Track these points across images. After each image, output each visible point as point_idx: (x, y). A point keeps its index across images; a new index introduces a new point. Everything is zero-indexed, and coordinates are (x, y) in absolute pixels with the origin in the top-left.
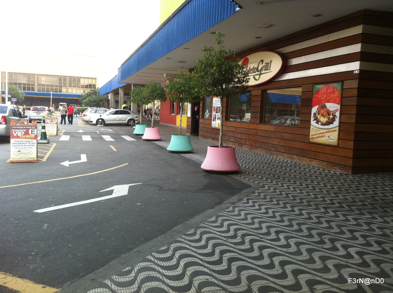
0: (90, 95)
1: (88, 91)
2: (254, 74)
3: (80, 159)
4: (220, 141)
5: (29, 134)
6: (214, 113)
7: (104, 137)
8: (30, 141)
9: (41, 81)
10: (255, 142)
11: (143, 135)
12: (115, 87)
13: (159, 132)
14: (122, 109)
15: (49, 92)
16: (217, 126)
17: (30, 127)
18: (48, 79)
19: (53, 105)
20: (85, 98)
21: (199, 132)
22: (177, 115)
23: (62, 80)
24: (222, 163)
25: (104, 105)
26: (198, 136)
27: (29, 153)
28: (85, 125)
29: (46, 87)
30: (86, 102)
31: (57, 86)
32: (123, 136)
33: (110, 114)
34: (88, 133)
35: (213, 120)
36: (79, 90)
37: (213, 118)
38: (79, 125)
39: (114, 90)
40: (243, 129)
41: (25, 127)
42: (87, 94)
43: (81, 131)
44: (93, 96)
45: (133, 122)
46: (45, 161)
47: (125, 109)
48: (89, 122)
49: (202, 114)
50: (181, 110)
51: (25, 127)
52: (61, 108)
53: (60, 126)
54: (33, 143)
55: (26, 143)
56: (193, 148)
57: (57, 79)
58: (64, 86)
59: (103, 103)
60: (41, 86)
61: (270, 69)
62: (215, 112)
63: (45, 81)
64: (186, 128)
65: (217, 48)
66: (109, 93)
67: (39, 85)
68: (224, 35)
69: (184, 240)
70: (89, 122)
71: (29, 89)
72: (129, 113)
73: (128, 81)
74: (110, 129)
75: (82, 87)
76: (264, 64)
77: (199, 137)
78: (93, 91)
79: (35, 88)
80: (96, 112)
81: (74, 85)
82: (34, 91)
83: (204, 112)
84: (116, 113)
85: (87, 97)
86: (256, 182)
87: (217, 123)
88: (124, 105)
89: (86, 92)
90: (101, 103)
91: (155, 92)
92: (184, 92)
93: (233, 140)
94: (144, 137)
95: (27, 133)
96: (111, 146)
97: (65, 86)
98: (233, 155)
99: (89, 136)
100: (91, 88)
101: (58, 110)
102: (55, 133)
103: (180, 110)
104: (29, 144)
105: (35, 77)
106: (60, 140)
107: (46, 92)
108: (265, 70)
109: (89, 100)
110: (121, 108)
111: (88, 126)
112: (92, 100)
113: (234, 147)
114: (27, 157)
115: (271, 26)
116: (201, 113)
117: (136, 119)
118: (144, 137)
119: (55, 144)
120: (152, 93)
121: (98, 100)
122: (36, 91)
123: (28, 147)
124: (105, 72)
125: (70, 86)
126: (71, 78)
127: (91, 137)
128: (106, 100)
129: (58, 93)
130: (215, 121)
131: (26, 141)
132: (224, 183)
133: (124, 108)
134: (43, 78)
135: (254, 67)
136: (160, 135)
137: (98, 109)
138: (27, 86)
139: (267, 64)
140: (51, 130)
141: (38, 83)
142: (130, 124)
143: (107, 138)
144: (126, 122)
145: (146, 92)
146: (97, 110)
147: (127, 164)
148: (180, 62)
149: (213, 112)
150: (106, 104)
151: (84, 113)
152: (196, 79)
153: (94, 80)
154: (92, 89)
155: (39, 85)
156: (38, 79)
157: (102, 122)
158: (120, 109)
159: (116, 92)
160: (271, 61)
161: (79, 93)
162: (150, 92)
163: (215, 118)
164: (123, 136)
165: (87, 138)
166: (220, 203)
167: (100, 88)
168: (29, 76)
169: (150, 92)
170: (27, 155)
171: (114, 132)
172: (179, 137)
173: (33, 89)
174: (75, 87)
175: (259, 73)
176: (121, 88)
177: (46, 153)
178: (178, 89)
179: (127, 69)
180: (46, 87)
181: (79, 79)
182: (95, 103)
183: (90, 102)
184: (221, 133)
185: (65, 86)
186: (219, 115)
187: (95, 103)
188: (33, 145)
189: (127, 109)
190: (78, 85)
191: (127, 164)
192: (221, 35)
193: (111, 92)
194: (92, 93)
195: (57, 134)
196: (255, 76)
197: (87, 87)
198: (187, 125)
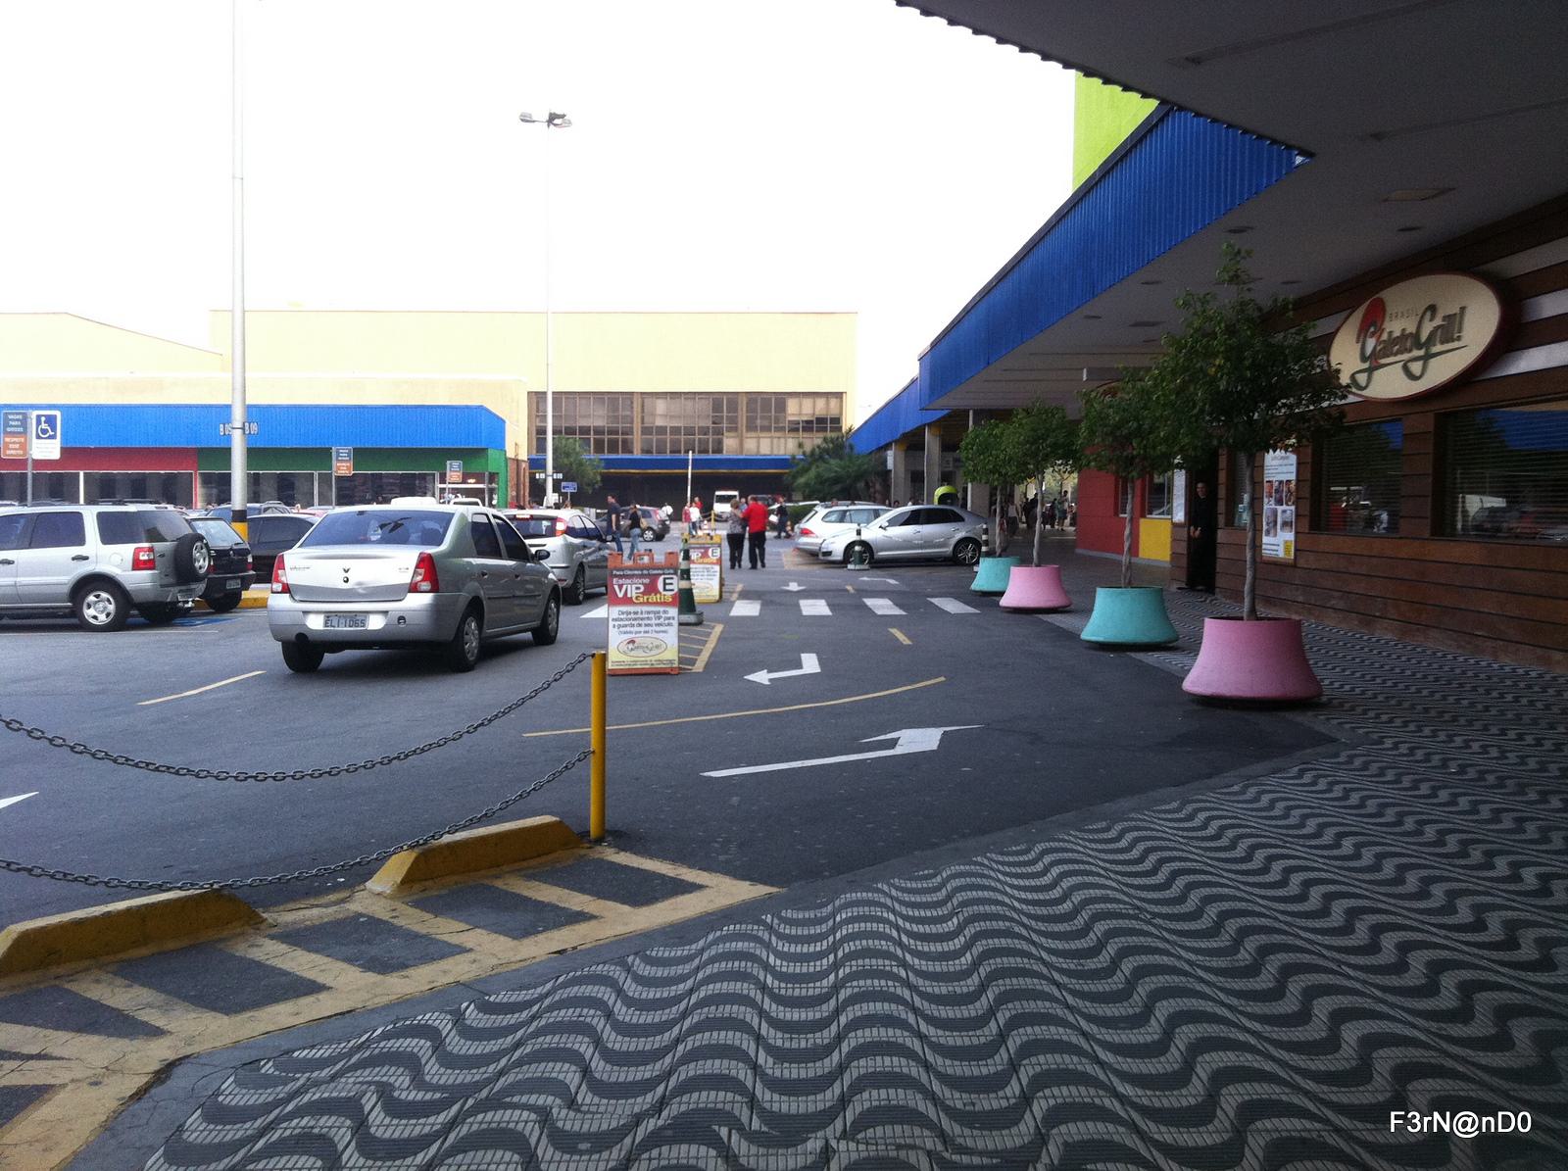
0: (821, 457)
1: (813, 441)
2: (1406, 356)
3: (799, 666)
4: (1247, 601)
5: (657, 591)
6: (1268, 505)
7: (869, 602)
8: (659, 612)
9: (653, 415)
10: (1418, 606)
11: (1001, 594)
12: (909, 424)
13: (1059, 580)
14: (935, 505)
15: (679, 452)
16: (1281, 554)
17: (660, 572)
18: (676, 406)
19: (697, 499)
20: (806, 470)
21: (1218, 577)
22: (1143, 516)
23: (724, 406)
24: (1251, 671)
25: (872, 490)
26: (1214, 594)
27: (657, 647)
28: (805, 568)
29: (668, 437)
30: (807, 484)
31: (704, 431)
32: (935, 601)
33: (892, 522)
34: (820, 591)
35: (1268, 533)
36: (782, 440)
37: (1268, 524)
38: (786, 568)
39: (905, 436)
40: (1374, 560)
41: (645, 572)
42: (813, 452)
43: (794, 587)
44: (832, 462)
45: (974, 550)
46: (701, 670)
47: (946, 504)
48: (821, 557)
49: (1227, 509)
50: (1129, 501)
51: (645, 572)
52: (720, 508)
53: (729, 576)
54: (669, 618)
55: (648, 618)
56: (1175, 631)
57: (706, 406)
58: (730, 430)
59: (867, 484)
60: (651, 434)
61: (1459, 338)
62: (1272, 502)
63: (666, 416)
64: (1168, 565)
65: (1227, 298)
66: (887, 446)
67: (646, 431)
68: (1249, 253)
69: (1074, 841)
70: (821, 557)
71: (613, 448)
72: (961, 519)
73: (954, 400)
74: (892, 577)
75: (794, 428)
76: (1438, 321)
77: (1218, 596)
78: (832, 441)
79: (632, 443)
80: (842, 520)
81: (766, 423)
82: (631, 452)
83: (1233, 500)
84: (913, 519)
85: (811, 464)
86: (1361, 731)
87: (1278, 543)
88: (940, 491)
89: (808, 448)
90: (861, 485)
91: (1045, 440)
92: (1136, 437)
93: (1341, 605)
94: (1004, 602)
95: (651, 589)
96: (895, 631)
97: (734, 429)
98: (1292, 645)
99: (823, 602)
100: (824, 430)
101: (713, 517)
102: (716, 592)
103: (1157, 498)
104: (658, 622)
105: (635, 405)
106: (732, 614)
107: (668, 456)
108: (1442, 343)
109: (818, 476)
110: (930, 501)
111: (816, 569)
112: (827, 475)
113: (1296, 617)
114: (653, 659)
115: (1444, 192)
116: (1222, 506)
117: (984, 537)
118: (1004, 602)
119: (719, 629)
120: (1032, 444)
121: (846, 469)
122: (637, 454)
123: (654, 628)
124: (872, 368)
125: (751, 427)
126: (753, 397)
127: (829, 605)
128: (878, 474)
129: (711, 456)
130: (1275, 535)
131: (649, 613)
132: (1236, 728)
133: (943, 499)
134: (661, 406)
135: (1404, 330)
136: (1066, 593)
137: (850, 508)
138: (606, 437)
139: (1448, 318)
140: (706, 583)
141: (643, 423)
142: (962, 557)
143: (882, 606)
144: (949, 550)
145: (1011, 439)
146: (846, 511)
147: (942, 679)
148: (1136, 325)
149: (1266, 500)
150: (878, 487)
151: (804, 525)
152: (1158, 398)
153: (833, 402)
154: (829, 434)
155: (646, 431)
156: (643, 411)
157: (862, 553)
158: (928, 503)
159: (912, 443)
160: (1463, 309)
161: (782, 452)
162: (1028, 442)
163: (1275, 522)
164: (935, 601)
165: (816, 608)
166: (1210, 776)
167: (856, 426)
168: (612, 400)
169: (1028, 442)
170: (653, 653)
171: (904, 588)
172: (1122, 593)
173: (627, 449)
174: (767, 429)
175: (1421, 353)
176: (930, 425)
177: (699, 653)
178: (1118, 427)
179: (955, 354)
180: (668, 437)
181: (780, 399)
182: (837, 488)
183: (822, 483)
184: (1249, 574)
185: (735, 429)
186: (1287, 511)
187: (837, 488)
188: (669, 624)
189: (951, 504)
190: (777, 420)
191: (942, 679)
192: (1239, 252)
193: (896, 442)
194: (826, 451)
195: (721, 596)
196: (1409, 364)
197: (808, 426)
198: (1174, 555)
